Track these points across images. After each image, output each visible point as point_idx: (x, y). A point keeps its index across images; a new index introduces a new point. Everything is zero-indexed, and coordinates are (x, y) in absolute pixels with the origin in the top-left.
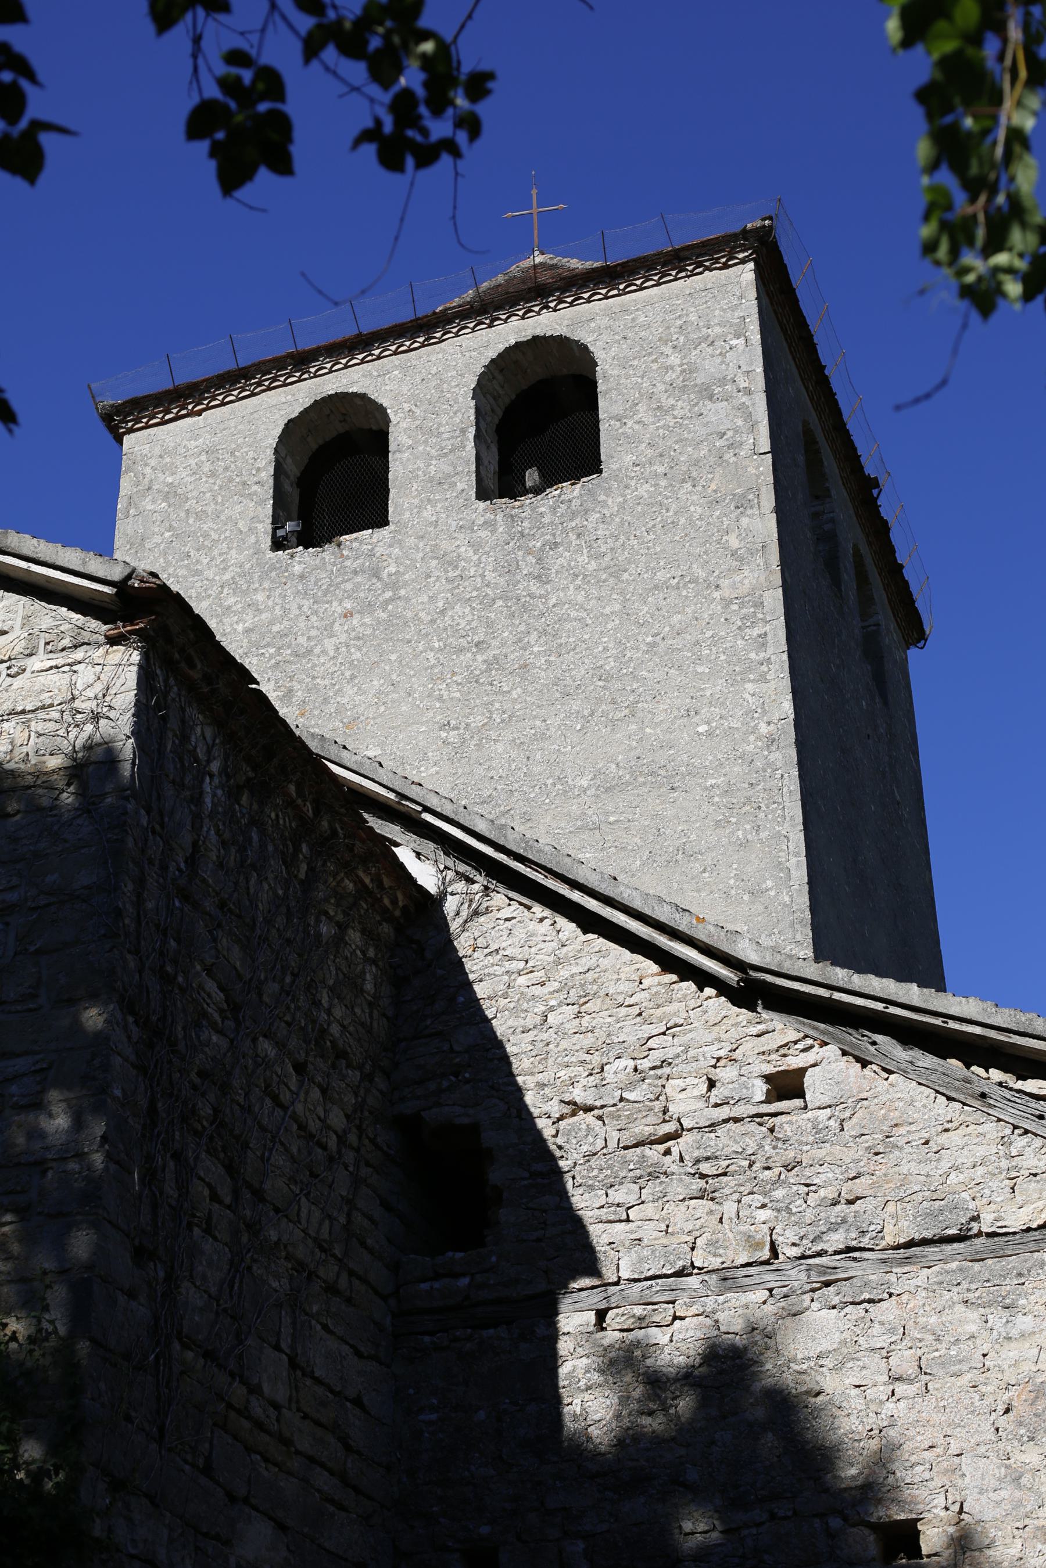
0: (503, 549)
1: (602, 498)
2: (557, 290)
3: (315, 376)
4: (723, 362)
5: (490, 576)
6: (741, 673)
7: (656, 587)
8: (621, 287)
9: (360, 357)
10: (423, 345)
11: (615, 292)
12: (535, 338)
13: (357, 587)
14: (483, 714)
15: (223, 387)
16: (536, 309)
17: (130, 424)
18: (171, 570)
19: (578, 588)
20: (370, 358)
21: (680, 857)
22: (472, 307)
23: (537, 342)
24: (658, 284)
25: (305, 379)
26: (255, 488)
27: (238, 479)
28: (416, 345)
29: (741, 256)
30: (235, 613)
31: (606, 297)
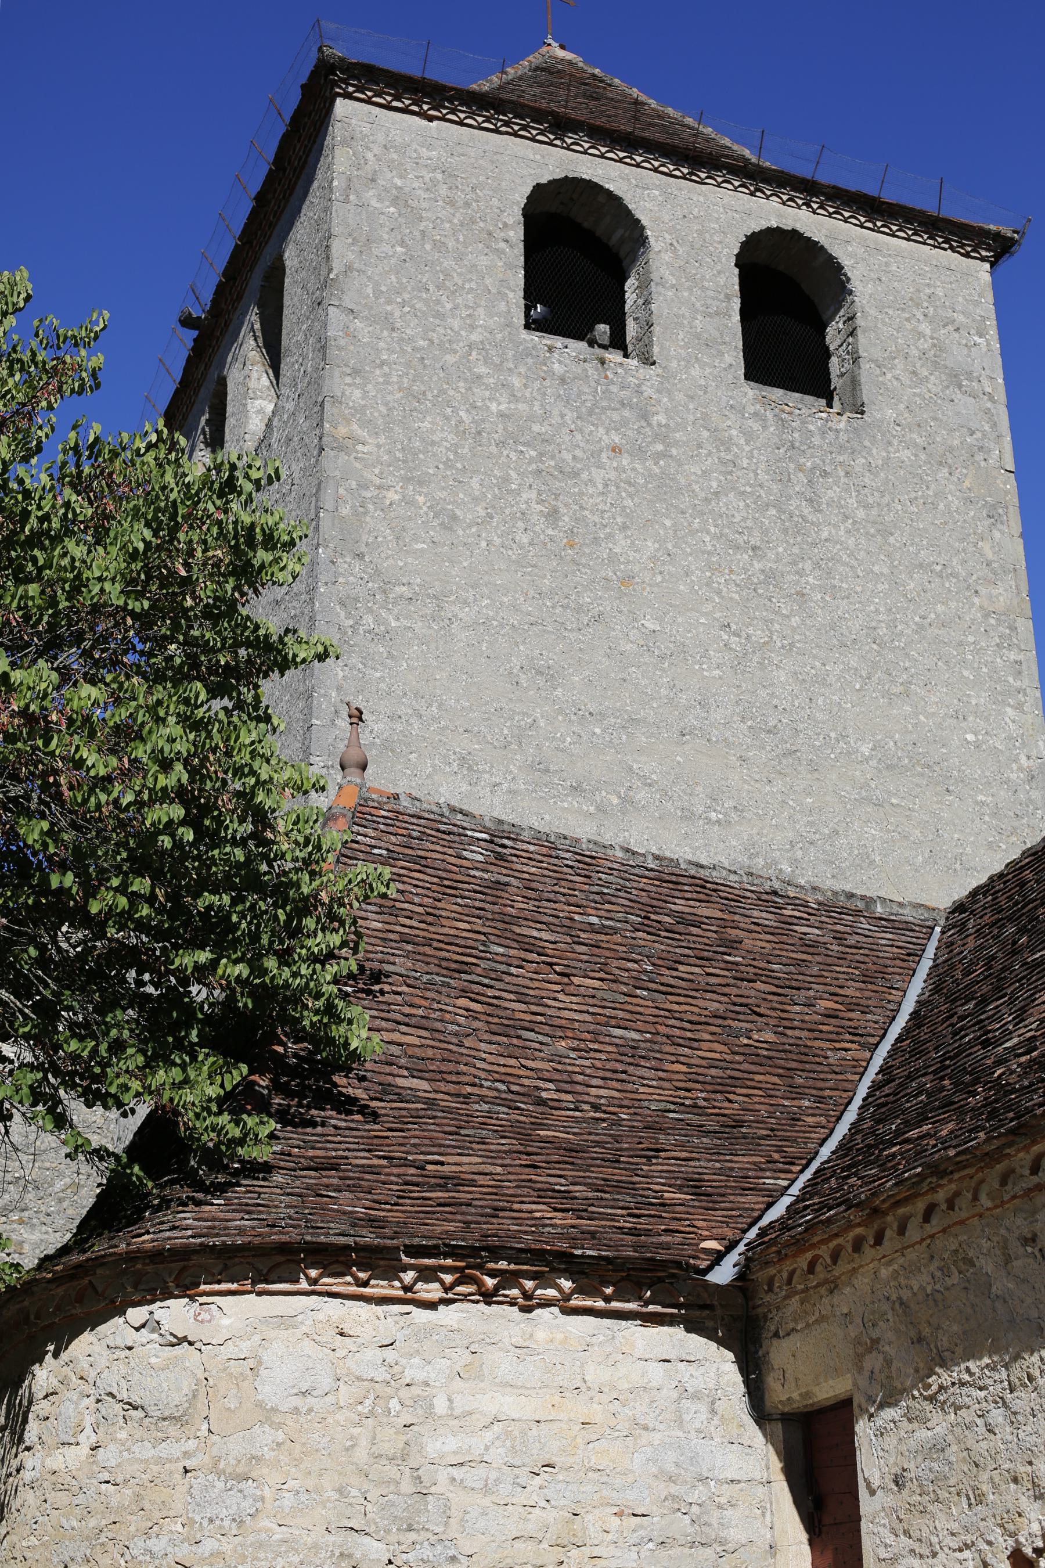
0: (773, 452)
1: (867, 443)
2: (824, 194)
3: (568, 148)
4: (969, 356)
5: (762, 476)
6: (1001, 693)
7: (921, 566)
8: (879, 224)
9: (622, 154)
10: (684, 178)
11: (870, 225)
12: (794, 232)
13: (624, 422)
14: (763, 631)
15: (469, 106)
16: (800, 202)
17: (351, 89)
18: (406, 296)
19: (848, 532)
20: (628, 160)
21: (958, 866)
22: (745, 166)
23: (794, 235)
24: (908, 239)
25: (556, 146)
26: (502, 245)
27: (482, 224)
28: (677, 173)
29: (984, 253)
30: (487, 387)
31: (862, 226)
